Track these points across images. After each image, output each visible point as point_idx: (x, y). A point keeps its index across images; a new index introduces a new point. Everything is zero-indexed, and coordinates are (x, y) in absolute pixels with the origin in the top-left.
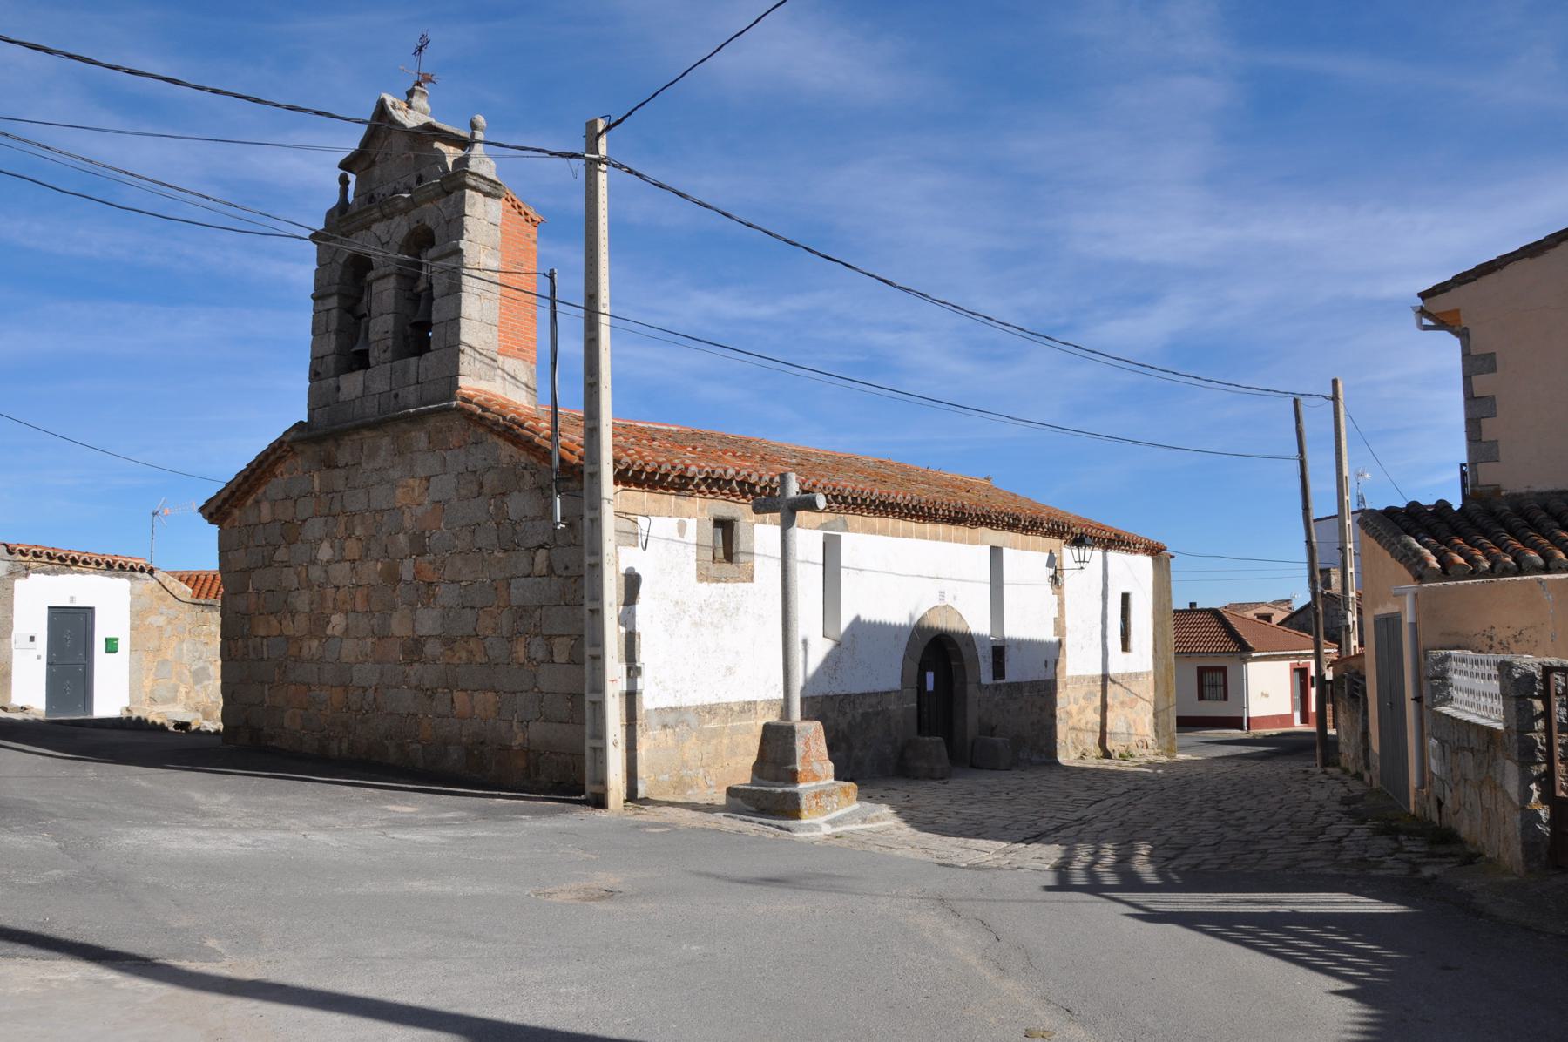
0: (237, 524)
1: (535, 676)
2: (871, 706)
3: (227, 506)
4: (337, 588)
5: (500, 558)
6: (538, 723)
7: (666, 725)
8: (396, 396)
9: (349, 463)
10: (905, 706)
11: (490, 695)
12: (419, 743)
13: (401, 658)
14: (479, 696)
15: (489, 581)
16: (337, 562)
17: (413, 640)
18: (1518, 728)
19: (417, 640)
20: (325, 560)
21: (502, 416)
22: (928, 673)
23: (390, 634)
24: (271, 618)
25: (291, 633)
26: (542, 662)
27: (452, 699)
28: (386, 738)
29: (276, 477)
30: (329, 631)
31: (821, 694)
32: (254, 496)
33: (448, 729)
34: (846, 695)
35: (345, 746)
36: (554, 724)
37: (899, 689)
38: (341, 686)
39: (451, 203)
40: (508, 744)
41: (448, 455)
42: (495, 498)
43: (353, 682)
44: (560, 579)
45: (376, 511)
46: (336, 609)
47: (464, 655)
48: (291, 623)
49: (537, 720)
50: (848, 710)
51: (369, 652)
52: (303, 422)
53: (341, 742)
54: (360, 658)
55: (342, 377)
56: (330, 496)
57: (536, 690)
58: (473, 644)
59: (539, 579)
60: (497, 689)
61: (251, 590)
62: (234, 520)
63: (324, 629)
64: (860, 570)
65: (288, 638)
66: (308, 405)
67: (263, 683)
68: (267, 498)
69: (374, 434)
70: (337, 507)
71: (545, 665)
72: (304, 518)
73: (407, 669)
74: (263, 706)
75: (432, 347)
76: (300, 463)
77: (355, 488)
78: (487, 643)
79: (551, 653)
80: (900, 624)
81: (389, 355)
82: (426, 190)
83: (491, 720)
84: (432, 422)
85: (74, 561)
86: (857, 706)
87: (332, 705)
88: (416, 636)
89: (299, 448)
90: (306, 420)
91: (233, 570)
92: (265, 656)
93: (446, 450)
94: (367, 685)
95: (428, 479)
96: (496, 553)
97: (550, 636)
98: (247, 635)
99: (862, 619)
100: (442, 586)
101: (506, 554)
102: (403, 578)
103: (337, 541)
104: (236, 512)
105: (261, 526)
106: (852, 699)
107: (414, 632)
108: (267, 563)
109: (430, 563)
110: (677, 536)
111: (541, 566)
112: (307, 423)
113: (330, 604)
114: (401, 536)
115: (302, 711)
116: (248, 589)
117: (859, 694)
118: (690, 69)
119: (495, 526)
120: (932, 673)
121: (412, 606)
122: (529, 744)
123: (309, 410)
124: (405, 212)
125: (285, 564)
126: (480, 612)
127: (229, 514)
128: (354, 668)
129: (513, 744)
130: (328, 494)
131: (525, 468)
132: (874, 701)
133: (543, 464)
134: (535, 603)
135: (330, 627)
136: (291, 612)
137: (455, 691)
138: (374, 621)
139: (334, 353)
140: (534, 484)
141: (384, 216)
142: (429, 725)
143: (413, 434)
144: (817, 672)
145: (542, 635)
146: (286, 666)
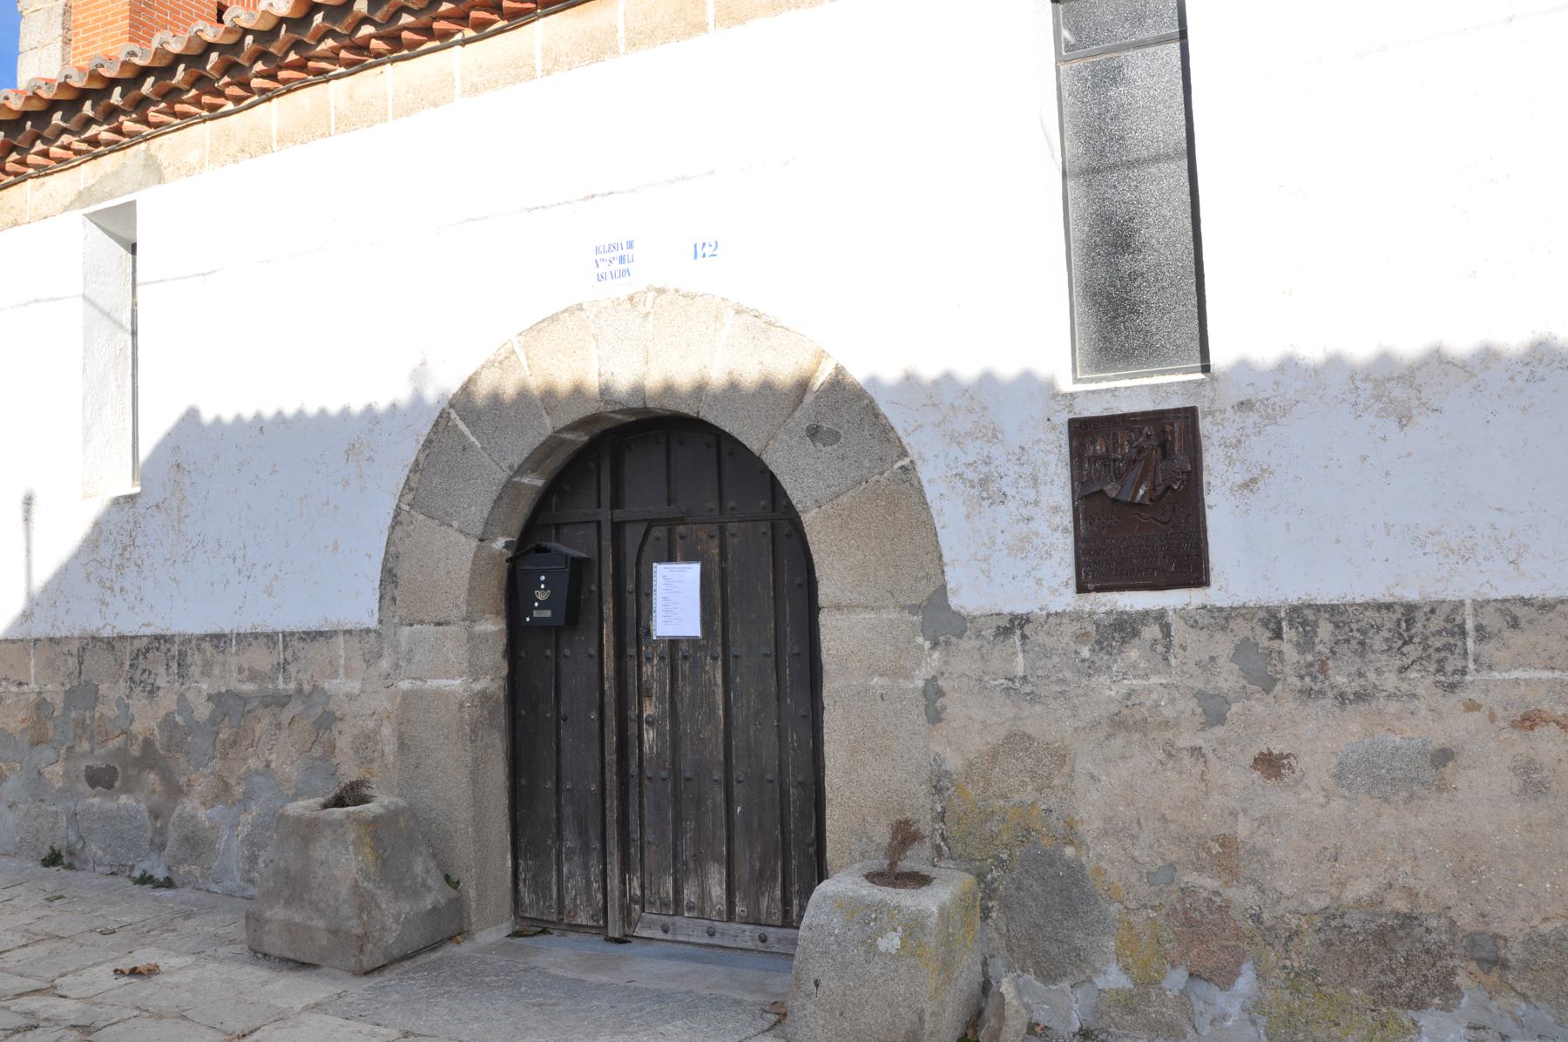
2: (254, 676)
7: (1390, 888)
10: (405, 685)
18: (324, 692)
22: (663, 574)
31: (77, 633)
34: (157, 638)
37: (373, 624)
50: (161, 682)
64: (108, 315)
80: (238, 419)
85: (28, 504)
86: (195, 671)
99: (207, 416)
106: (175, 650)
117: (203, 638)
120: (692, 571)
128: (1235, 707)
132: (262, 659)
144: (63, 575)
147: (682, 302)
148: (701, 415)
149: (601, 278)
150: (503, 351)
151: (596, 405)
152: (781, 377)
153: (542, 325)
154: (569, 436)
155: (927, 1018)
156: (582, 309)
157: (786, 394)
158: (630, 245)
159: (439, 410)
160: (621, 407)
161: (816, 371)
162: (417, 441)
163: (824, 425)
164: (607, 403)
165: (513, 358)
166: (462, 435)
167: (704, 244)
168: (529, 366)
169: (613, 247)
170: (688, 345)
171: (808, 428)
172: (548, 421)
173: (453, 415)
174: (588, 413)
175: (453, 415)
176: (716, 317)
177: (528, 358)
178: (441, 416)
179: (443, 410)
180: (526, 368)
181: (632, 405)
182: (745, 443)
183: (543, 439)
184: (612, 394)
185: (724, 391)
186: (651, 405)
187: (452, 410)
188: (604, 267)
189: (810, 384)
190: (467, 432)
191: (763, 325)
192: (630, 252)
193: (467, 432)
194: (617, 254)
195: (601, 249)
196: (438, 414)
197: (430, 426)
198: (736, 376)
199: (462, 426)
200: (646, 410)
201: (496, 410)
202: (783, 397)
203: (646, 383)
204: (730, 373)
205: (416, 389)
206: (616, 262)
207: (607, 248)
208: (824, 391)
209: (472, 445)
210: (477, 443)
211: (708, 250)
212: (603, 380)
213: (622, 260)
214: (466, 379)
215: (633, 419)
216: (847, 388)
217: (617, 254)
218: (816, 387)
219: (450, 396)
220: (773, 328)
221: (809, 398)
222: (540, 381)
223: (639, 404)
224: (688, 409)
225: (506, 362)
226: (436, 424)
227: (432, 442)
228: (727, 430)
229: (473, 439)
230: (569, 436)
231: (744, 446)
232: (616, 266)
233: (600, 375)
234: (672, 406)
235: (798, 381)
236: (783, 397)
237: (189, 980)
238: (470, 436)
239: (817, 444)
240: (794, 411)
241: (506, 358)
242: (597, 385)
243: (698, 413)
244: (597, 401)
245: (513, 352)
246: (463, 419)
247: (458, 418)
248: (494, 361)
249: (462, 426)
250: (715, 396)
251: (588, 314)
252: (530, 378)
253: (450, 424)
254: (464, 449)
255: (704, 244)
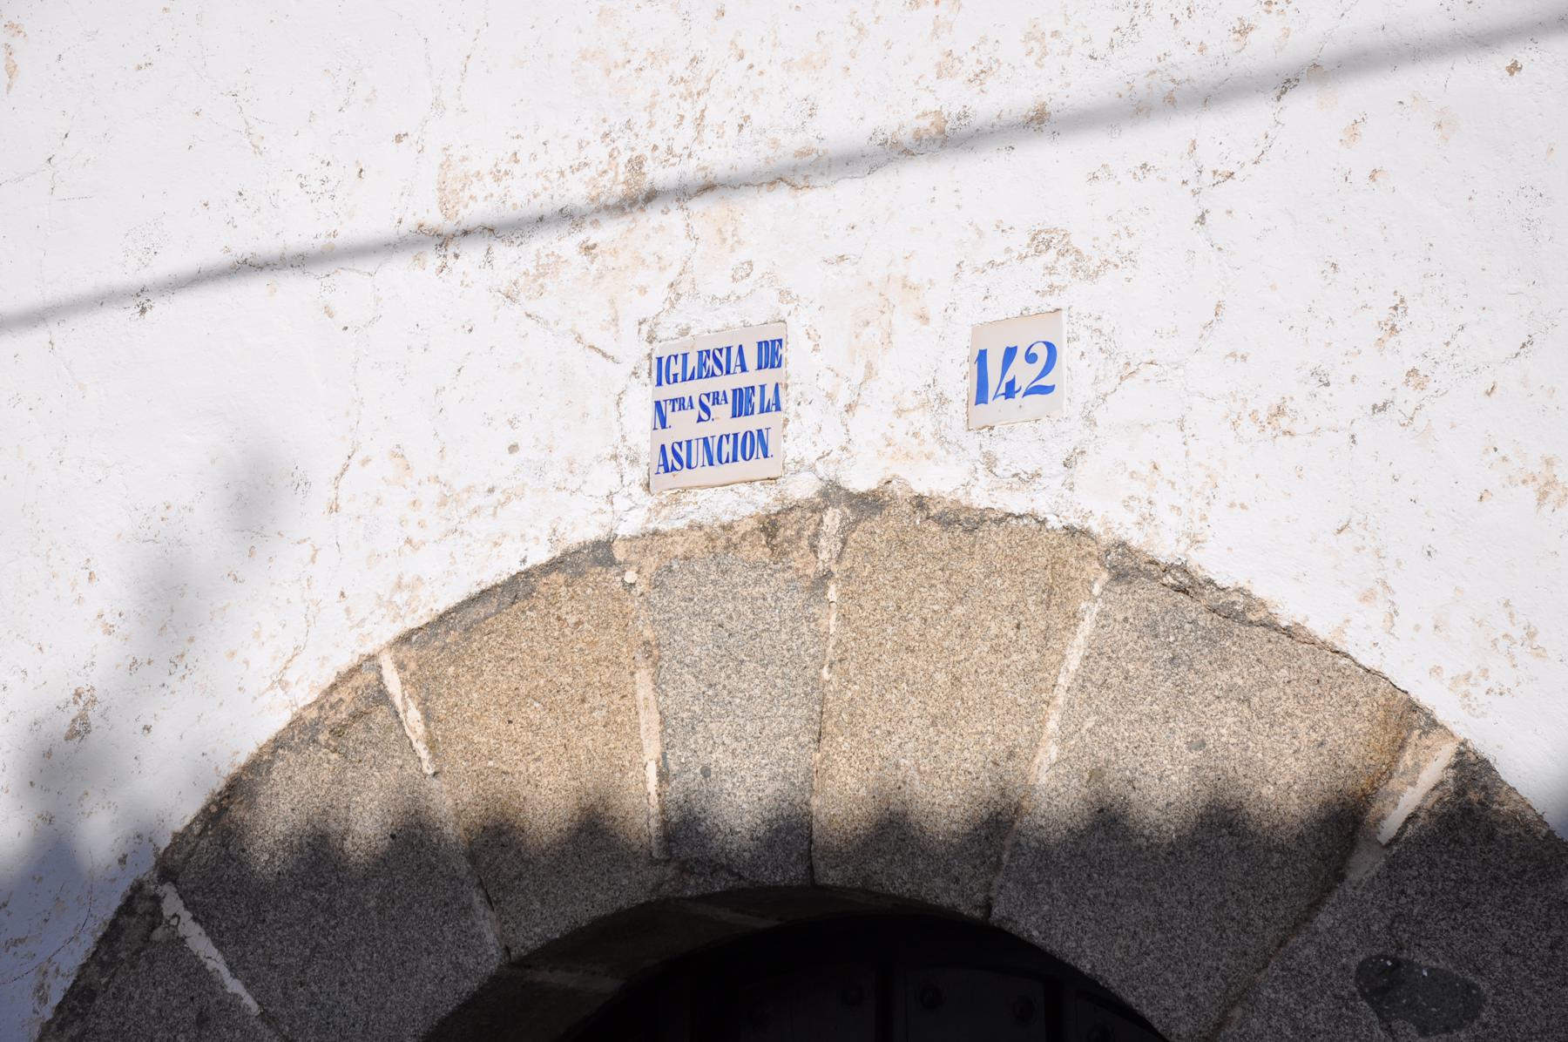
147: (937, 539)
148: (998, 912)
149: (672, 460)
150: (344, 693)
151: (652, 875)
152: (1268, 791)
153: (480, 610)
154: (557, 978)
155: (477, 899)
156: (609, 561)
157: (1282, 850)
158: (770, 354)
159: (124, 887)
160: (732, 882)
161: (1389, 774)
162: (41, 993)
163: (1420, 958)
164: (685, 868)
165: (380, 716)
166: (199, 969)
167: (1010, 353)
168: (432, 744)
169: (714, 361)
170: (956, 680)
171: (1362, 966)
172: (489, 930)
173: (172, 904)
174: (623, 902)
175: (172, 904)
176: (1050, 591)
177: (427, 716)
178: (127, 908)
179: (138, 888)
180: (424, 753)
181: (772, 876)
182: (1148, 1012)
183: (469, 985)
184: (704, 838)
185: (1077, 836)
186: (831, 877)
187: (168, 890)
188: (684, 426)
189: (1370, 817)
190: (215, 961)
191: (1205, 620)
192: (769, 377)
193: (215, 961)
194: (725, 384)
195: (676, 368)
196: (117, 902)
197: (88, 943)
198: (1114, 785)
199: (200, 943)
200: (813, 890)
201: (317, 888)
202: (1276, 858)
203: (816, 802)
204: (1097, 774)
205: (50, 820)
206: (723, 411)
207: (693, 362)
208: (1420, 842)
209: (230, 1005)
210: (249, 1000)
211: (1023, 373)
212: (675, 790)
213: (742, 402)
214: (219, 784)
215: (770, 923)
216: (1501, 832)
217: (725, 384)
218: (1394, 819)
219: (165, 842)
220: (1237, 629)
221: (1364, 867)
222: (467, 794)
223: (794, 874)
224: (942, 894)
225: (357, 732)
226: (112, 934)
227: (92, 996)
228: (1086, 966)
229: (234, 986)
230: (557, 978)
231: (1143, 1023)
232: (723, 421)
233: (663, 776)
234: (899, 881)
235: (1326, 804)
236: (1276, 858)
237: (344, 716)
238: (224, 971)
239: (1397, 1024)
240: (1315, 906)
241: (355, 717)
242: (655, 808)
243: (988, 907)
244: (654, 862)
245: (382, 697)
246: (203, 917)
247: (186, 916)
248: (315, 726)
249: (200, 943)
250: (1044, 852)
251: (630, 577)
252: (435, 784)
253: (158, 934)
254: (202, 1020)
255: (1010, 353)
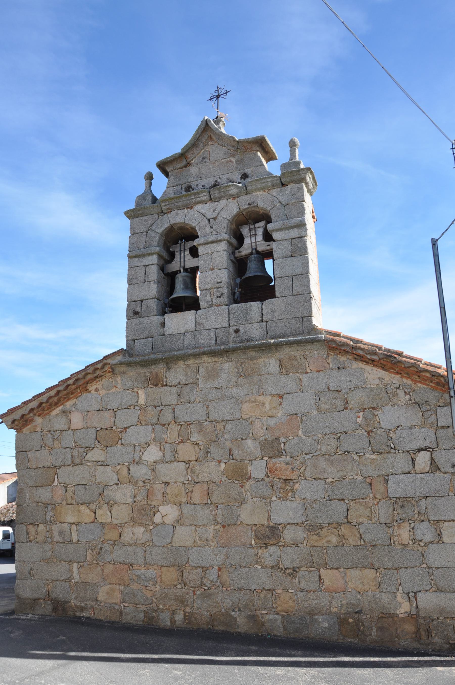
0: (38, 429)
1: (423, 555)
3: (31, 415)
4: (167, 484)
5: (374, 460)
6: (429, 593)
8: (237, 331)
9: (182, 383)
11: (370, 573)
12: (277, 614)
13: (253, 542)
14: (354, 573)
15: (360, 478)
16: (167, 462)
17: (268, 527)
19: (272, 527)
20: (152, 461)
21: (377, 347)
23: (239, 523)
24: (83, 508)
25: (109, 520)
26: (431, 542)
27: (320, 576)
28: (234, 611)
29: (90, 392)
30: (157, 519)
32: (62, 406)
33: (316, 602)
35: (179, 617)
36: (448, 594)
38: (174, 566)
39: (288, 192)
40: (392, 612)
41: (305, 378)
42: (364, 411)
43: (190, 562)
44: (446, 475)
45: (217, 421)
46: (165, 500)
47: (334, 539)
48: (108, 512)
49: (427, 591)
51: (211, 536)
52: (123, 349)
53: (173, 613)
54: (199, 543)
55: (167, 316)
56: (159, 408)
57: (425, 566)
58: (344, 530)
59: (421, 475)
60: (376, 566)
61: (56, 483)
62: (36, 426)
63: (151, 519)
65: (103, 524)
66: (127, 337)
67: (70, 562)
68: (77, 410)
69: (216, 359)
70: (167, 417)
71: (435, 545)
72: (125, 426)
73: (260, 551)
74: (70, 581)
75: (277, 294)
76: (119, 381)
77: (190, 402)
78: (362, 529)
79: (440, 535)
81: (224, 299)
82: (263, 181)
83: (370, 593)
84: (286, 352)
87: (161, 581)
88: (271, 524)
89: (123, 368)
90: (125, 348)
91: (34, 466)
92: (75, 539)
93: (302, 373)
94: (207, 565)
95: (281, 396)
96: (367, 455)
97: (438, 522)
98: (51, 521)
100: (303, 483)
101: (380, 456)
102: (253, 476)
103: (168, 445)
104: (39, 420)
105: (70, 432)
107: (269, 519)
108: (77, 461)
109: (287, 463)
110: (451, 428)
111: (423, 465)
112: (126, 350)
113: (159, 496)
114: (249, 442)
115: (122, 587)
116: (53, 482)
118: (430, 119)
119: (366, 434)
121: (267, 499)
122: (418, 612)
123: (127, 340)
124: (235, 197)
125: (100, 463)
126: (352, 503)
127: (32, 421)
129: (398, 612)
130: (155, 407)
131: (399, 388)
133: (419, 385)
134: (418, 494)
135: (158, 516)
136: (108, 503)
137: (322, 569)
138: (219, 512)
139: (155, 298)
140: (410, 400)
141: (211, 199)
142: (291, 598)
143: (261, 360)
145: (429, 521)
146: (101, 549)
